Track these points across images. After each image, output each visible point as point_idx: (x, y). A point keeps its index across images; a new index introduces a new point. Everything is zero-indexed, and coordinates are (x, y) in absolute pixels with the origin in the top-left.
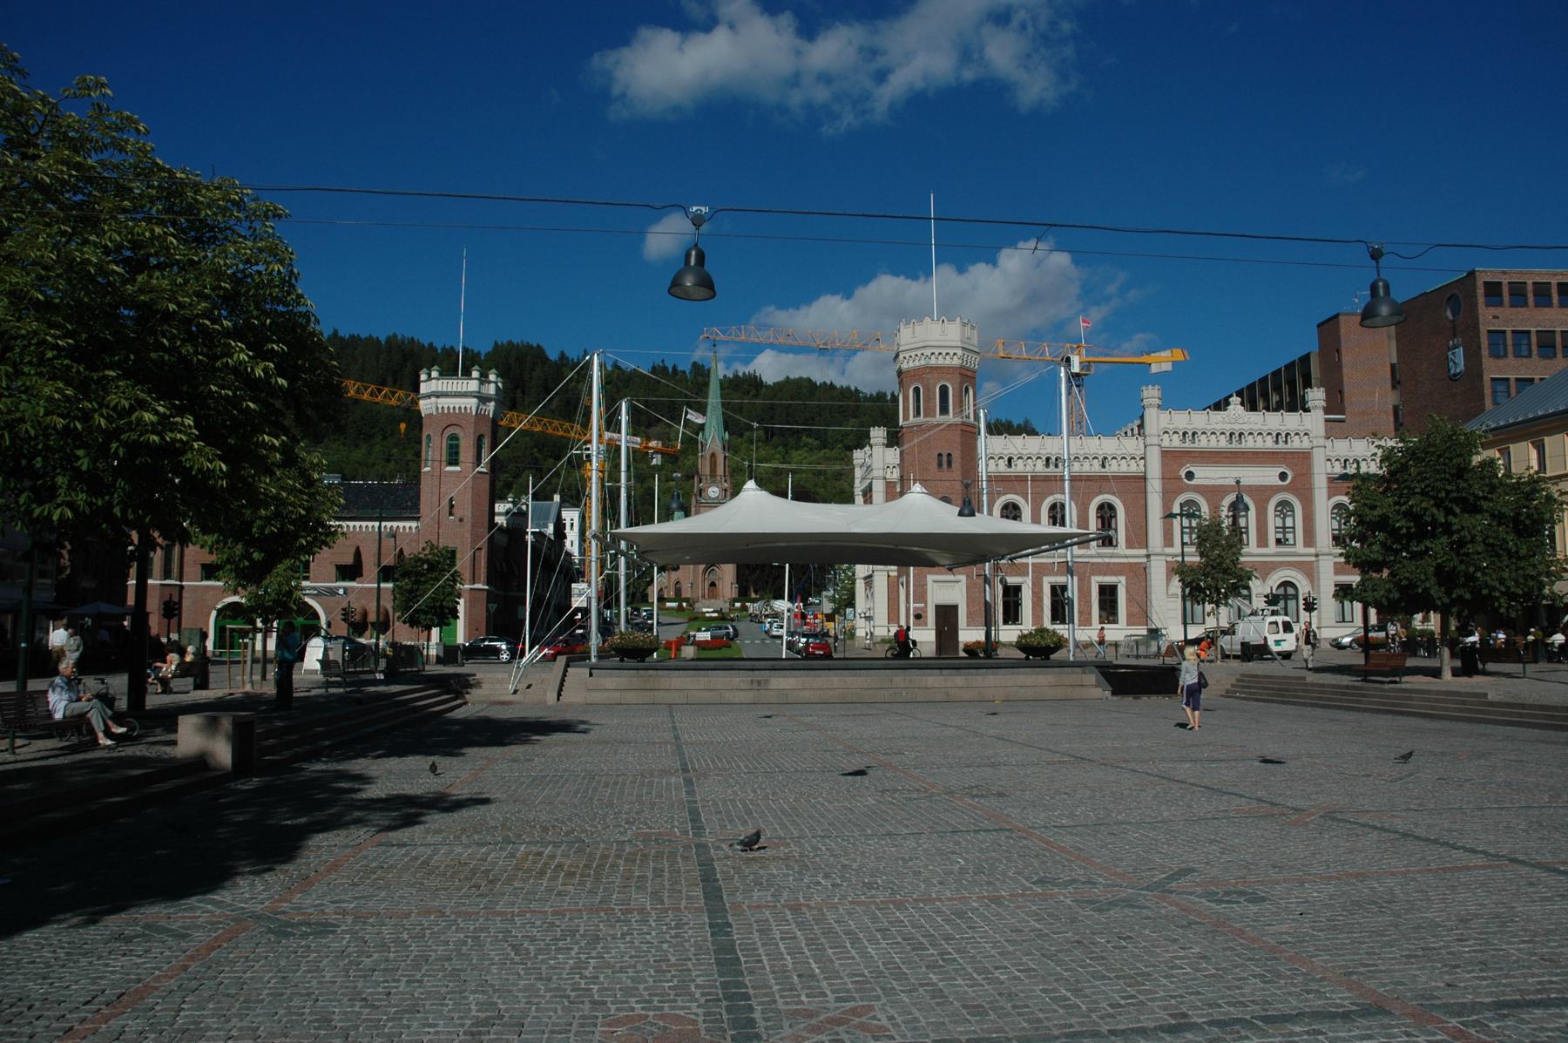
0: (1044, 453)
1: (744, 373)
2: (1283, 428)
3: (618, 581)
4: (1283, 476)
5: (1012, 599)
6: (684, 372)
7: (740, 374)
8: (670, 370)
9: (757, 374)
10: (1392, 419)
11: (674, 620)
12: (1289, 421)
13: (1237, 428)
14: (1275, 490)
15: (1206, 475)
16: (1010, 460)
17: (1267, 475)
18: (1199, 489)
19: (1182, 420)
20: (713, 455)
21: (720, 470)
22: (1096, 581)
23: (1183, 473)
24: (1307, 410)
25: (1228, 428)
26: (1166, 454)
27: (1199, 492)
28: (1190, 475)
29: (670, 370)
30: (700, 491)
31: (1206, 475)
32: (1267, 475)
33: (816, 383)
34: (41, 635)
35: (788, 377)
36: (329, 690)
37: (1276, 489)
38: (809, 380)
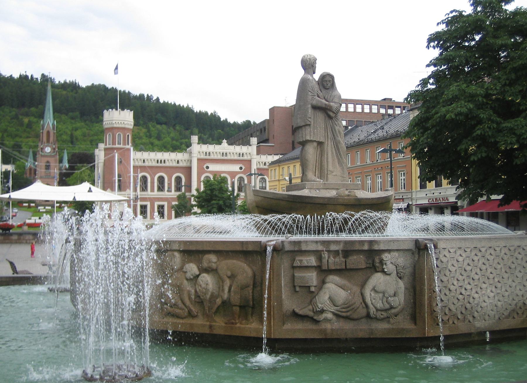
0: (156, 159)
1: (70, 81)
2: (241, 151)
3: (144, 329)
4: (241, 168)
5: (143, 210)
6: (37, 79)
7: (68, 81)
8: (30, 78)
9: (77, 82)
10: (291, 146)
11: (326, 153)
12: (244, 149)
13: (225, 151)
14: (237, 173)
15: (214, 167)
16: (144, 161)
17: (235, 168)
18: (210, 172)
19: (205, 148)
20: (48, 133)
21: (51, 139)
22: (156, 204)
23: (205, 167)
24: (250, 145)
25: (221, 151)
26: (199, 160)
27: (211, 174)
28: (208, 168)
29: (30, 78)
30: (42, 149)
31: (214, 167)
32: (235, 168)
33: (108, 88)
34: (465, 214)
35: (93, 84)
36: (184, 187)
37: (239, 173)
38: (104, 86)
